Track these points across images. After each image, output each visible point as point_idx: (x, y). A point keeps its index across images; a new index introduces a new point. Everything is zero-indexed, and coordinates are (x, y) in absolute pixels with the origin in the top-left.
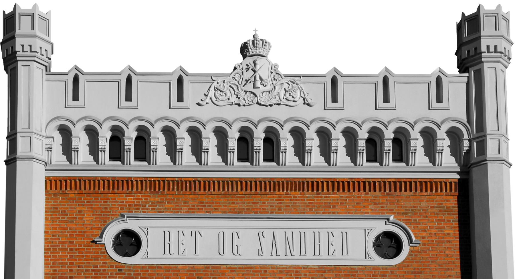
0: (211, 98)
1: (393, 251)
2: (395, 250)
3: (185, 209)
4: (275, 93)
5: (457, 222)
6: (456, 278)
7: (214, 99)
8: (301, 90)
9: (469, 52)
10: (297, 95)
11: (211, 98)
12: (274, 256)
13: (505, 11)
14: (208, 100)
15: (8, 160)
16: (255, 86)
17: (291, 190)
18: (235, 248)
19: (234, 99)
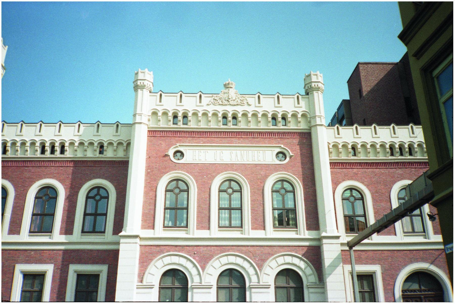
0: (212, 102)
1: (284, 159)
2: (284, 158)
3: (202, 142)
4: (236, 101)
5: (38, 217)
6: (142, 123)
7: (213, 103)
8: (246, 100)
9: (308, 87)
10: (245, 102)
11: (212, 102)
12: (243, 161)
13: (320, 73)
14: (211, 103)
15: (438, 200)
16: (324, 239)
17: (243, 136)
18: (221, 157)
19: (221, 103)
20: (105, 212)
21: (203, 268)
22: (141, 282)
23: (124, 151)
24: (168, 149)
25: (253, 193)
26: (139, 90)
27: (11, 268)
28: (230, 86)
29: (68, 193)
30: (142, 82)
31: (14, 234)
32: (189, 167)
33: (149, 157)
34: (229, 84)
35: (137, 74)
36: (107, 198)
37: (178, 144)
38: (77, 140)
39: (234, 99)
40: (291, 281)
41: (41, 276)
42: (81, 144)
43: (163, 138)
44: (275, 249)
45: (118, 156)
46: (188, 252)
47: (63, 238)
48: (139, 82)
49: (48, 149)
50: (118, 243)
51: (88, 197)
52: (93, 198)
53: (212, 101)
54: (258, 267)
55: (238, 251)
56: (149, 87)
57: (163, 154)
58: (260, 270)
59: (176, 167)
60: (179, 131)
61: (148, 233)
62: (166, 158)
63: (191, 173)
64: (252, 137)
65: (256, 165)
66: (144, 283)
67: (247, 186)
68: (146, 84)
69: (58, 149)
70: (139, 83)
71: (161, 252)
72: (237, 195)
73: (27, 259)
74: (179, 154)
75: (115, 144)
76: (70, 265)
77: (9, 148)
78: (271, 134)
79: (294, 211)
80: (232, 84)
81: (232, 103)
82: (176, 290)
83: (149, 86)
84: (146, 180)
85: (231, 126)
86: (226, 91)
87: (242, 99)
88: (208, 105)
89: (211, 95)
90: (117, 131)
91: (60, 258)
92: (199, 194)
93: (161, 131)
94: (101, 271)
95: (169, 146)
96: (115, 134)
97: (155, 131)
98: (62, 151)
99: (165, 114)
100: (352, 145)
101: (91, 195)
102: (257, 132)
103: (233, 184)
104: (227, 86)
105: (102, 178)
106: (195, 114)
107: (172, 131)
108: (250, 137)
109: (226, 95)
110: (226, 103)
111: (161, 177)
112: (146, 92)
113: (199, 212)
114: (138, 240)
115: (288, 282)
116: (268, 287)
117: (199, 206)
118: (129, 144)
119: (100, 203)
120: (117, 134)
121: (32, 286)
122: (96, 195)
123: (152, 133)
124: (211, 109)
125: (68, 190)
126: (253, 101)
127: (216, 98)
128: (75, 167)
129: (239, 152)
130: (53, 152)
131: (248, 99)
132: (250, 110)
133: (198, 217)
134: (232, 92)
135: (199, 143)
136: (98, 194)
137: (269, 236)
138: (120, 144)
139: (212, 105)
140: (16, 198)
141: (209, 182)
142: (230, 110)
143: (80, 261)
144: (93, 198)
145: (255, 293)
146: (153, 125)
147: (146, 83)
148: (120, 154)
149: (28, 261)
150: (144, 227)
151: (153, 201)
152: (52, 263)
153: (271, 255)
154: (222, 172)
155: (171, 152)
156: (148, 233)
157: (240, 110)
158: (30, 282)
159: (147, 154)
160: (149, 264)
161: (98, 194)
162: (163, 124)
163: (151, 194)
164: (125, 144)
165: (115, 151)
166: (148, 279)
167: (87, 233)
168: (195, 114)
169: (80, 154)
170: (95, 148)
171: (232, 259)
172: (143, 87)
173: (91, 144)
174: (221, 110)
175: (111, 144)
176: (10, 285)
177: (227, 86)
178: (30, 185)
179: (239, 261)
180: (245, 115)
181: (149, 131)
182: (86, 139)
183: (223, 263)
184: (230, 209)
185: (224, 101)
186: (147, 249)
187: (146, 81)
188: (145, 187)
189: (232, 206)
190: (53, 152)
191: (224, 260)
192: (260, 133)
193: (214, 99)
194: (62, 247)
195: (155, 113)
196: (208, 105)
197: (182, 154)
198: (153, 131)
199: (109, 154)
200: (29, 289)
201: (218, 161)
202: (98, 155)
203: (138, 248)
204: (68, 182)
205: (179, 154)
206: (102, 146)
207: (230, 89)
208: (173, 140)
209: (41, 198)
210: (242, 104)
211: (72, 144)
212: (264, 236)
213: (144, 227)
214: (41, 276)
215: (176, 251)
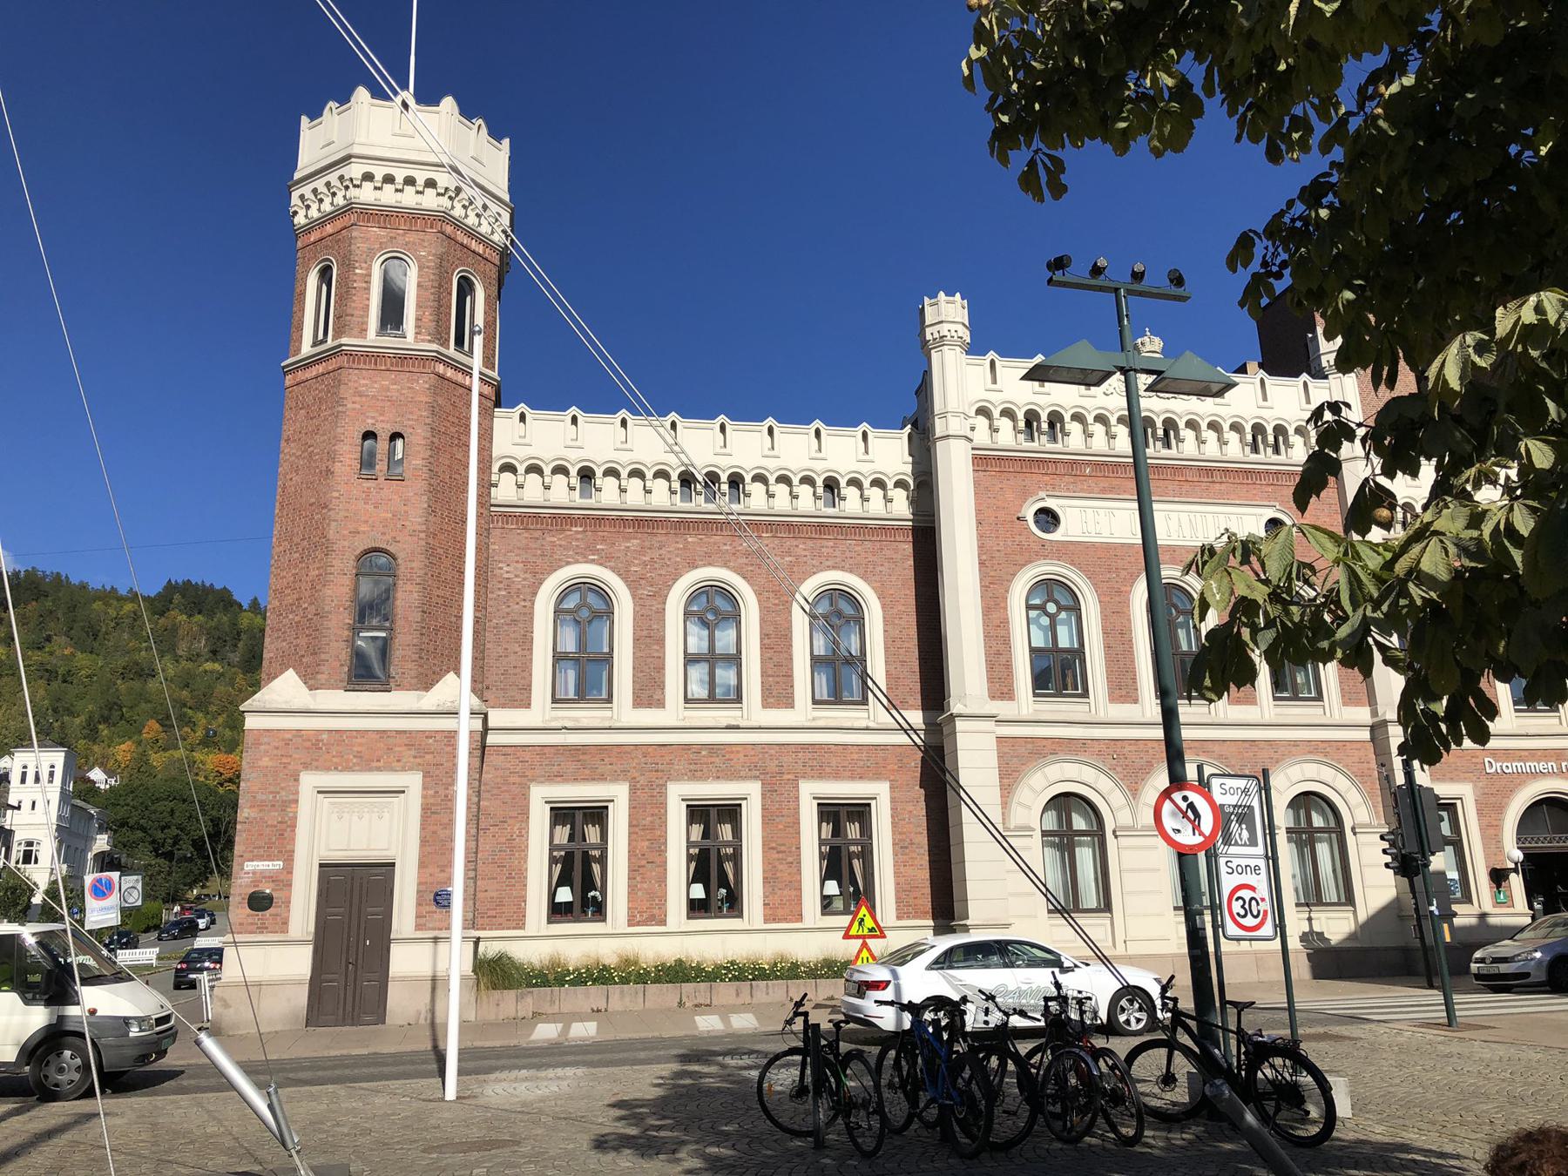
20: (606, 650)
32: (1072, 552)
41: (860, 812)
56: (956, 338)
61: (1002, 708)
64: (1210, 480)
68: (946, 333)
73: (692, 767)
76: (301, 774)
78: (1248, 475)
79: (1079, 653)
83: (953, 334)
95: (1025, 495)
96: (719, 450)
99: (1008, 413)
100: (680, 475)
108: (1206, 480)
123: (983, 461)
140: (639, 618)
141: (1123, 589)
143: (821, 774)
147: (944, 329)
149: (695, 775)
152: (756, 778)
155: (1029, 513)
161: (583, 604)
162: (1007, 436)
175: (855, 482)
181: (975, 458)
183: (1294, 780)
187: (944, 324)
192: (1226, 471)
205: (1048, 518)
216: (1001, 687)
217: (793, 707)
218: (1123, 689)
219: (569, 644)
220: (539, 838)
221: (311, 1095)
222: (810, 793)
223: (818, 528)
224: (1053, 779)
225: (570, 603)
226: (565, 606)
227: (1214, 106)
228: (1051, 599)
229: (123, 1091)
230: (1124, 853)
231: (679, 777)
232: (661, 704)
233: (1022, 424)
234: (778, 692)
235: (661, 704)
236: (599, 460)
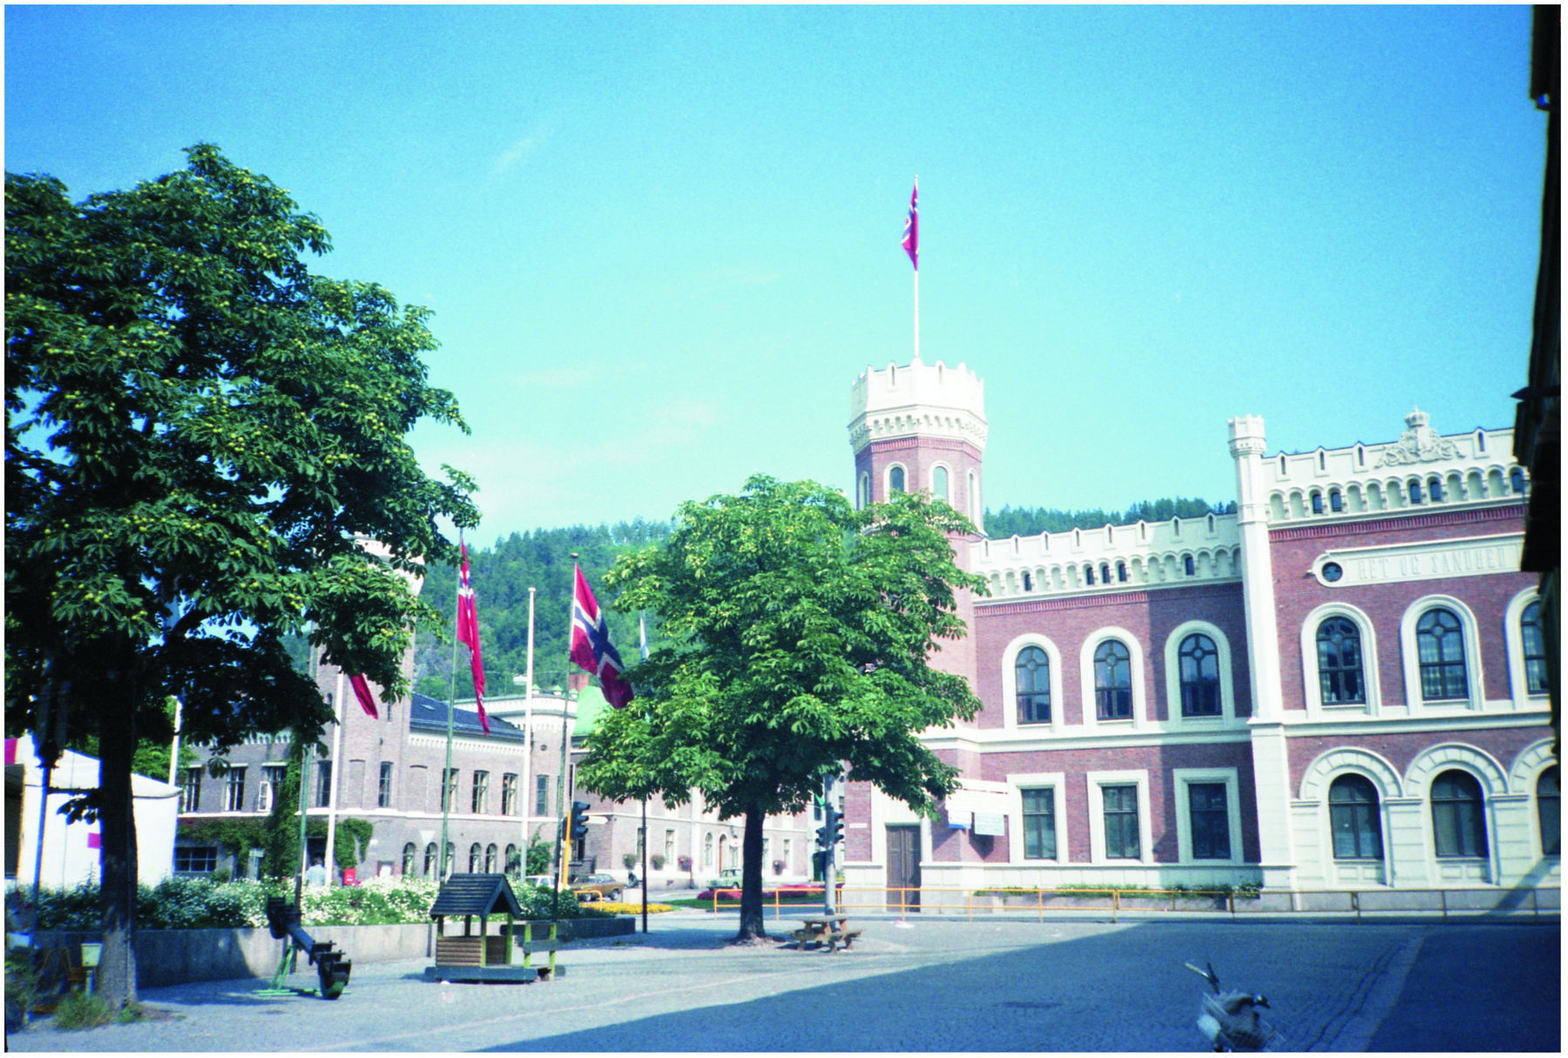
10: (1452, 451)
19: (1402, 460)
21: (1402, 771)
22: (1297, 796)
23: (1231, 565)
24: (1309, 564)
25: (1483, 633)
26: (1241, 458)
27: (1081, 778)
28: (1418, 422)
29: (1149, 649)
30: (1244, 442)
31: (1073, 723)
32: (1356, 594)
33: (1278, 581)
34: (1414, 419)
35: (1232, 426)
36: (1215, 652)
37: (1328, 551)
38: (1145, 555)
39: (1429, 448)
40: (1460, 791)
41: (1130, 790)
42: (1153, 560)
43: (1297, 543)
44: (1533, 732)
45: (1220, 576)
46: (1372, 746)
47: (1156, 727)
48: (1238, 445)
49: (1097, 574)
50: (1248, 732)
51: (1181, 655)
52: (1190, 654)
53: (1385, 458)
54: (1502, 762)
55: (1463, 740)
57: (1301, 574)
58: (1508, 770)
59: (1330, 595)
60: (1328, 526)
61: (1296, 717)
62: (1309, 581)
63: (1359, 604)
65: (1486, 577)
66: (1303, 798)
67: (1470, 620)
69: (1114, 572)
70: (1238, 446)
71: (1325, 747)
72: (1452, 637)
74: (1332, 569)
75: (1212, 556)
77: (1033, 580)
80: (1421, 418)
81: (1425, 457)
82: (1358, 809)
84: (1278, 624)
85: (1428, 504)
86: (1412, 433)
87: (1445, 446)
88: (1377, 467)
89: (1381, 447)
90: (1211, 529)
91: (1157, 759)
92: (1380, 643)
93: (1293, 530)
94: (1227, 778)
95: (1313, 556)
97: (1282, 531)
98: (1123, 577)
101: (1187, 648)
102: (1483, 510)
103: (1443, 617)
104: (1412, 424)
105: (1200, 619)
106: (1354, 489)
107: (1313, 528)
109: (1412, 443)
110: (1414, 458)
111: (1306, 615)
112: (1254, 459)
113: (1384, 674)
114: (1281, 730)
115: (1352, 797)
116: (1523, 799)
117: (1381, 664)
118: (1237, 552)
119: (1203, 663)
120: (1213, 535)
121: (1120, 806)
122: (1195, 649)
123: (1279, 536)
124: (1383, 477)
125: (1148, 643)
126: (1467, 446)
127: (1391, 452)
128: (1151, 602)
129: (1449, 555)
130: (1106, 579)
131: (1457, 444)
132: (1463, 467)
133: (1382, 683)
134: (1424, 436)
135: (1369, 544)
136: (1197, 647)
137: (1519, 710)
138: (1221, 553)
139: (1385, 467)
142: (1423, 472)
144: (1190, 654)
145: (1500, 809)
146: (1277, 521)
147: (1251, 442)
148: (1225, 573)
150: (1288, 706)
151: (1295, 661)
153: (1525, 743)
154: (1419, 596)
155: (1317, 568)
156: (1296, 717)
157: (1442, 470)
158: (1031, 802)
159: (1274, 575)
160: (1306, 768)
161: (1197, 647)
163: (1293, 647)
164: (1230, 554)
165: (1214, 567)
166: (1307, 792)
167: (1388, 918)
168: (1354, 489)
169: (1153, 581)
170: (1178, 566)
171: (1454, 754)
172: (1247, 453)
173: (1170, 558)
174: (1403, 474)
175: (1204, 554)
176: (1084, 804)
177: (1412, 424)
178: (1082, 641)
179: (1467, 756)
180: (1454, 477)
181: (1270, 532)
182: (1160, 552)
184: (1442, 664)
185: (1409, 455)
186: (1301, 743)
188: (1279, 636)
189: (1446, 659)
190: (1106, 579)
191: (1440, 756)
193: (1388, 454)
194: (1159, 742)
195: (1276, 497)
196: (1377, 467)
197: (1338, 569)
198: (1278, 531)
199: (1204, 575)
200: (1116, 810)
201: (1410, 577)
202: (1185, 578)
203: (1283, 744)
204: (1145, 627)
205: (1333, 570)
206: (1188, 559)
207: (1419, 429)
208: (1318, 544)
209: (1104, 660)
210: (1446, 458)
211: (1137, 562)
212: (1509, 711)
213: (1288, 706)
214: (1130, 790)
215: (1350, 744)
216: (1295, 695)
217: (1003, 726)
218: (1499, 686)
219: (1432, 655)
220: (1096, 805)
221: (881, 964)
222: (1097, 778)
223: (1184, 591)
224: (1335, 765)
225: (1188, 648)
226: (1184, 650)
227: (46, 394)
228: (1438, 624)
229: (1031, 950)
230: (1498, 814)
231: (1096, 768)
232: (1080, 721)
233: (1406, 493)
234: (1395, 692)
235: (1080, 721)
236: (1194, 549)
